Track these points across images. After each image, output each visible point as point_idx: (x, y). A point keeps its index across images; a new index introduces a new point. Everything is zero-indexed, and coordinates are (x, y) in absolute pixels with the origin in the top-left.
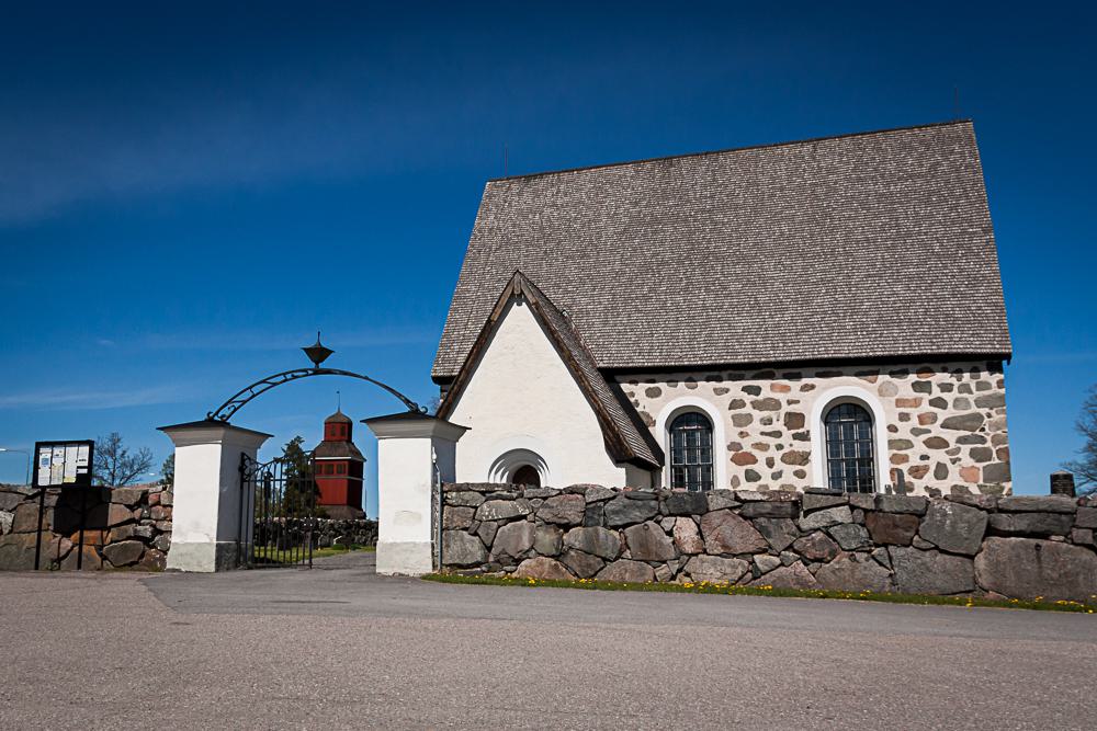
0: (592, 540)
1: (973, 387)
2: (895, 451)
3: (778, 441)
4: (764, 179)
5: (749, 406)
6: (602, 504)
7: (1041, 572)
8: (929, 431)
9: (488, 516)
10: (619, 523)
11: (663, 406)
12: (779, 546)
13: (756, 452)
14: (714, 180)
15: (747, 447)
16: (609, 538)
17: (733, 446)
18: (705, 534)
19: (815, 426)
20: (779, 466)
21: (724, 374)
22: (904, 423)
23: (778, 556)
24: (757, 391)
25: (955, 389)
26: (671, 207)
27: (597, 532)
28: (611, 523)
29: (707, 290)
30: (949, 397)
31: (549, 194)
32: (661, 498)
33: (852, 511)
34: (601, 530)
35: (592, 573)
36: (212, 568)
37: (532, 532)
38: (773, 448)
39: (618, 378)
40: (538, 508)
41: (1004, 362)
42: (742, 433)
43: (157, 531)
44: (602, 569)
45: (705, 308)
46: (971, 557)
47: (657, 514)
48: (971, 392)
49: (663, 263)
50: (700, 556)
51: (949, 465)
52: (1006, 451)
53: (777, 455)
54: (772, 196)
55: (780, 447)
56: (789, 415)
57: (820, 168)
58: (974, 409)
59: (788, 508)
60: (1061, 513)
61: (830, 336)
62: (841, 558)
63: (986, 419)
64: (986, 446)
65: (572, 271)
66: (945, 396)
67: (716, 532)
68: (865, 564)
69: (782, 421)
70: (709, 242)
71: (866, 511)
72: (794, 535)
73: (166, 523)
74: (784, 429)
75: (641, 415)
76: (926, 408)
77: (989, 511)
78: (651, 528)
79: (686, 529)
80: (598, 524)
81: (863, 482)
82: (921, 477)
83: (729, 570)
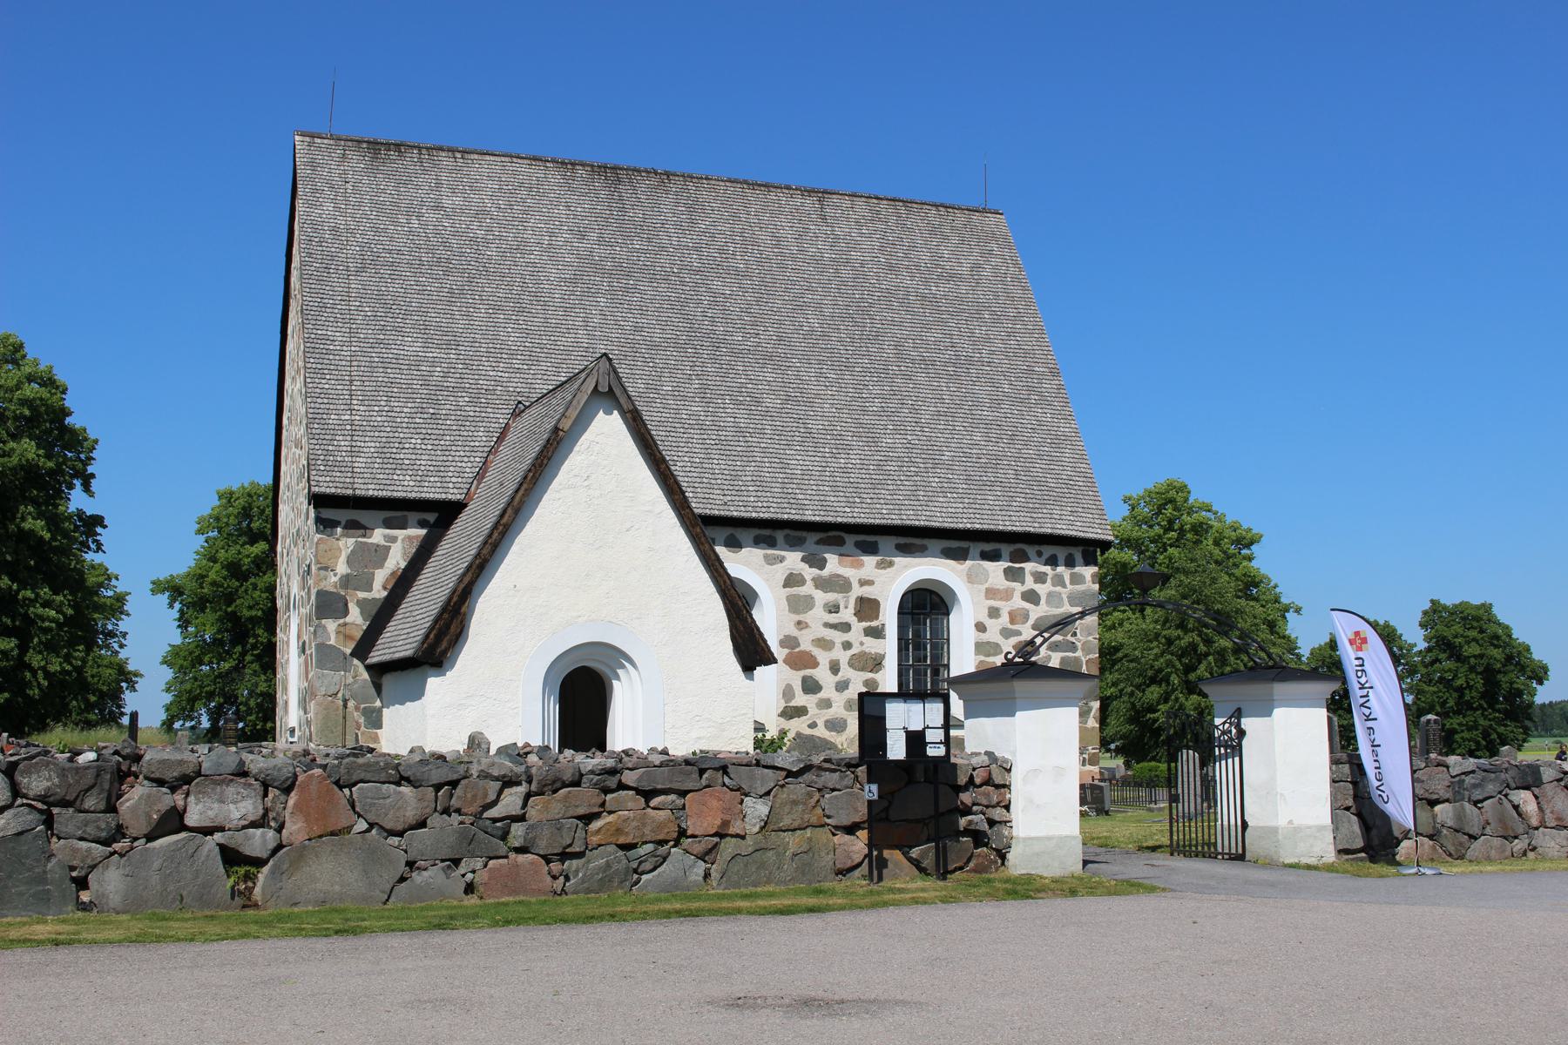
1: (1067, 581)
2: (982, 658)
4: (764, 237)
5: (809, 583)
8: (1019, 633)
13: (817, 652)
15: (806, 645)
19: (889, 617)
21: (780, 535)
24: (821, 564)
25: (1049, 580)
30: (1042, 590)
38: (838, 646)
39: (711, 532)
42: (799, 623)
45: (740, 431)
48: (1064, 586)
53: (843, 657)
57: (837, 237)
64: (1076, 655)
69: (851, 609)
74: (853, 620)
76: (1018, 603)
79: (1525, 799)
80: (1463, 799)
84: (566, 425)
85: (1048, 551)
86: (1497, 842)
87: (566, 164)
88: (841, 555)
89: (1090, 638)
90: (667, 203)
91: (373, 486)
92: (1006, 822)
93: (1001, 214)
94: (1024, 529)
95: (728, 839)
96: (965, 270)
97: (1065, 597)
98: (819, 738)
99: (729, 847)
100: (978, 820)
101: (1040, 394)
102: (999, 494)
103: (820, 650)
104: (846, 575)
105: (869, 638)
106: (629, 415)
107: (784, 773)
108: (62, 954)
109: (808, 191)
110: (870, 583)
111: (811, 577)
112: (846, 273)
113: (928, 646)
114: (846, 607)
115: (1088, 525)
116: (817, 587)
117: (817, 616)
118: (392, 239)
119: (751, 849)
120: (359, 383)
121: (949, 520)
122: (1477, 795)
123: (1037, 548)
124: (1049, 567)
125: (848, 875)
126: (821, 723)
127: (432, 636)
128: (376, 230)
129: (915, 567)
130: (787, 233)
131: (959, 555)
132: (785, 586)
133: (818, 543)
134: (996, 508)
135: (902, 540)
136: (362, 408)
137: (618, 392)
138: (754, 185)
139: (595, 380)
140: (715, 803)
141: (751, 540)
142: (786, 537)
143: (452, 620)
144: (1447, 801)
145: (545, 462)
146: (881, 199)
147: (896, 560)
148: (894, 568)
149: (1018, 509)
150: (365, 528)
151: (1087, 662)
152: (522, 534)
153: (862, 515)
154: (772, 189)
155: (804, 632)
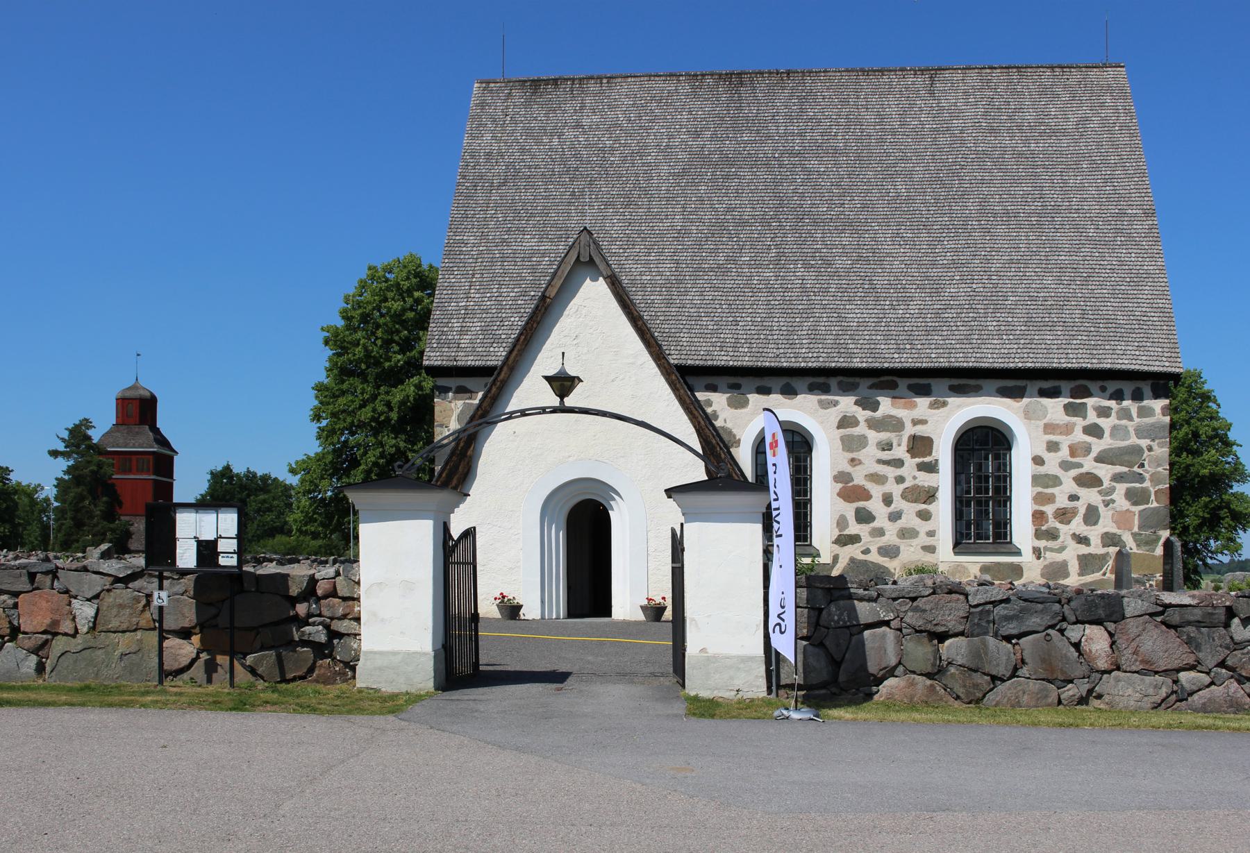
1: (1134, 414)
2: (1040, 489)
3: (899, 472)
4: (870, 117)
5: (863, 424)
8: (1080, 465)
9: (838, 622)
10: (1014, 632)
11: (750, 421)
12: (1210, 662)
13: (870, 486)
15: (859, 479)
16: (1000, 653)
19: (944, 454)
20: (899, 504)
21: (833, 382)
22: (1052, 454)
23: (1208, 673)
24: (874, 407)
25: (1114, 414)
26: (745, 142)
27: (984, 644)
29: (807, 266)
30: (1105, 423)
32: (1064, 601)
34: (991, 641)
37: (899, 642)
38: (891, 480)
40: (906, 612)
42: (853, 460)
43: (333, 635)
48: (1131, 419)
49: (743, 223)
50: (1113, 674)
51: (1101, 508)
53: (896, 490)
55: (900, 480)
56: (914, 439)
57: (942, 109)
58: (1133, 440)
59: (1221, 615)
61: (968, 337)
64: (1144, 485)
67: (1134, 644)
69: (904, 447)
72: (1228, 648)
74: (906, 457)
76: (1079, 436)
78: (1055, 639)
79: (1096, 640)
80: (986, 633)
82: (1069, 522)
83: (1151, 691)
84: (552, 292)
85: (1112, 386)
86: (1034, 686)
87: (697, 76)
88: (894, 397)
89: (1160, 469)
91: (472, 358)
92: (356, 635)
93: (1123, 67)
94: (1080, 365)
95: (60, 637)
96: (1070, 125)
98: (872, 563)
99: (59, 645)
100: (317, 633)
101: (1129, 235)
102: (1059, 333)
104: (899, 416)
105: (922, 473)
106: (609, 280)
107: (111, 579)
108: (757, 721)
109: (922, 70)
110: (923, 422)
111: (864, 418)
112: (943, 140)
113: (991, 479)
114: (899, 445)
115: (1155, 358)
116: (870, 427)
117: (870, 454)
118: (533, 157)
119: (80, 648)
120: (479, 276)
121: (1000, 360)
122: (1011, 628)
123: (1100, 383)
124: (1114, 402)
125: (179, 677)
126: (874, 549)
127: (444, 475)
128: (523, 151)
132: (839, 427)
133: (871, 387)
134: (1053, 347)
135: (956, 382)
136: (477, 295)
137: (597, 260)
139: (576, 252)
140: (44, 604)
142: (840, 383)
143: (460, 462)
144: (962, 634)
145: (535, 326)
146: (995, 68)
147: (950, 400)
148: (949, 406)
149: (1077, 347)
150: (471, 392)
151: (1156, 492)
153: (910, 360)
154: (886, 73)
155: (858, 468)
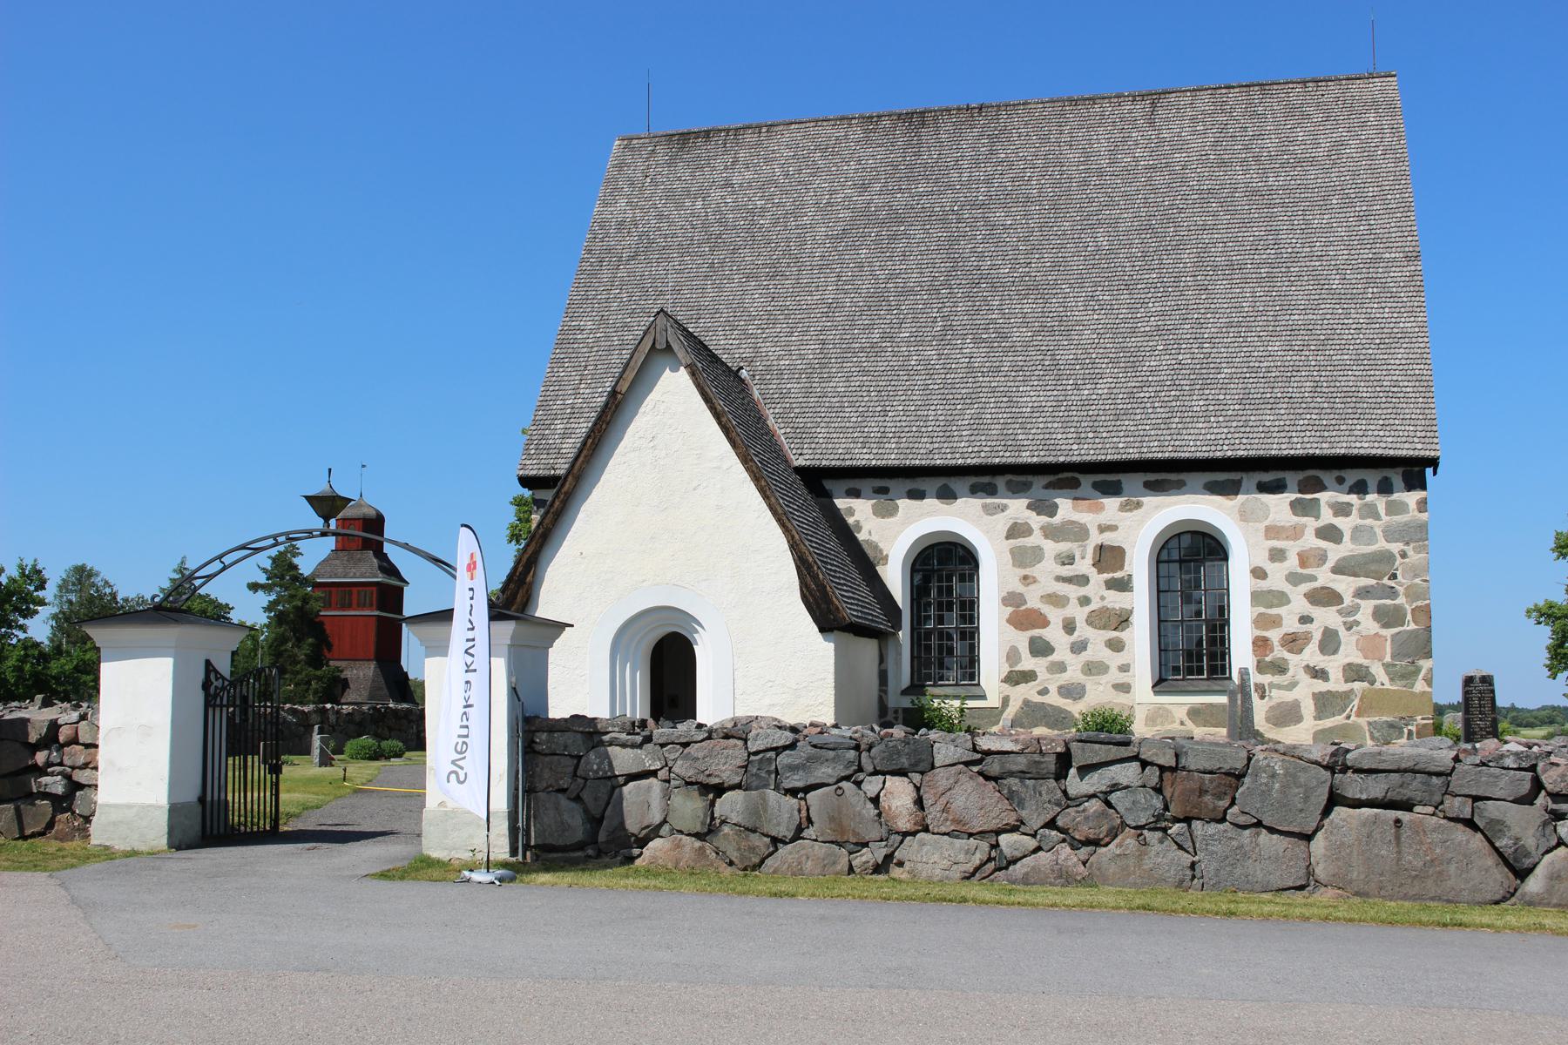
0: (757, 811)
2: (1262, 610)
3: (1083, 591)
4: (1073, 156)
5: (1037, 534)
6: (772, 754)
7: (1399, 860)
8: (1313, 578)
9: (596, 772)
10: (800, 784)
11: (900, 532)
12: (1035, 822)
14: (991, 152)
15: (1033, 602)
16: (781, 811)
17: (1013, 599)
18: (927, 803)
19: (1139, 567)
20: (1083, 631)
21: (1000, 482)
24: (1051, 510)
25: (1354, 511)
26: (921, 195)
27: (764, 799)
28: (787, 784)
29: (977, 341)
30: (1344, 524)
31: (720, 166)
32: (863, 747)
33: (1143, 769)
34: (772, 795)
35: (756, 860)
36: (156, 834)
37: (667, 796)
38: (1074, 602)
39: (828, 485)
41: (1429, 471)
42: (1025, 577)
44: (771, 854)
45: (970, 369)
46: (1308, 838)
47: (856, 772)
48: (1377, 517)
49: (905, 292)
51: (1342, 632)
52: (1427, 611)
54: (1085, 183)
55: (1085, 601)
57: (1161, 140)
58: (1382, 544)
59: (1050, 763)
60: (1430, 774)
61: (1166, 422)
62: (1123, 840)
63: (1399, 560)
65: (756, 301)
66: (1340, 522)
68: (1158, 847)
69: (1089, 560)
70: (981, 256)
71: (1162, 769)
73: (87, 772)
74: (1092, 572)
75: (865, 546)
76: (1311, 541)
77: (1330, 768)
78: (847, 792)
79: (898, 794)
80: (766, 786)
81: (1212, 657)
82: (1300, 651)
83: (961, 857)
85: (1352, 476)
88: (1076, 499)
90: (971, 134)
97: (1379, 532)
98: (1051, 706)
100: (55, 784)
103: (1052, 607)
104: (1082, 521)
110: (1112, 528)
114: (1083, 558)
117: (1047, 569)
122: (796, 781)
123: (1336, 473)
126: (1053, 689)
128: (660, 217)
129: (1168, 506)
130: (1102, 147)
131: (1230, 489)
133: (1046, 487)
135: (1152, 477)
138: (1074, 102)
141: (966, 489)
142: (1008, 483)
143: (519, 589)
145: (604, 427)
147: (1145, 500)
152: (588, 501)
